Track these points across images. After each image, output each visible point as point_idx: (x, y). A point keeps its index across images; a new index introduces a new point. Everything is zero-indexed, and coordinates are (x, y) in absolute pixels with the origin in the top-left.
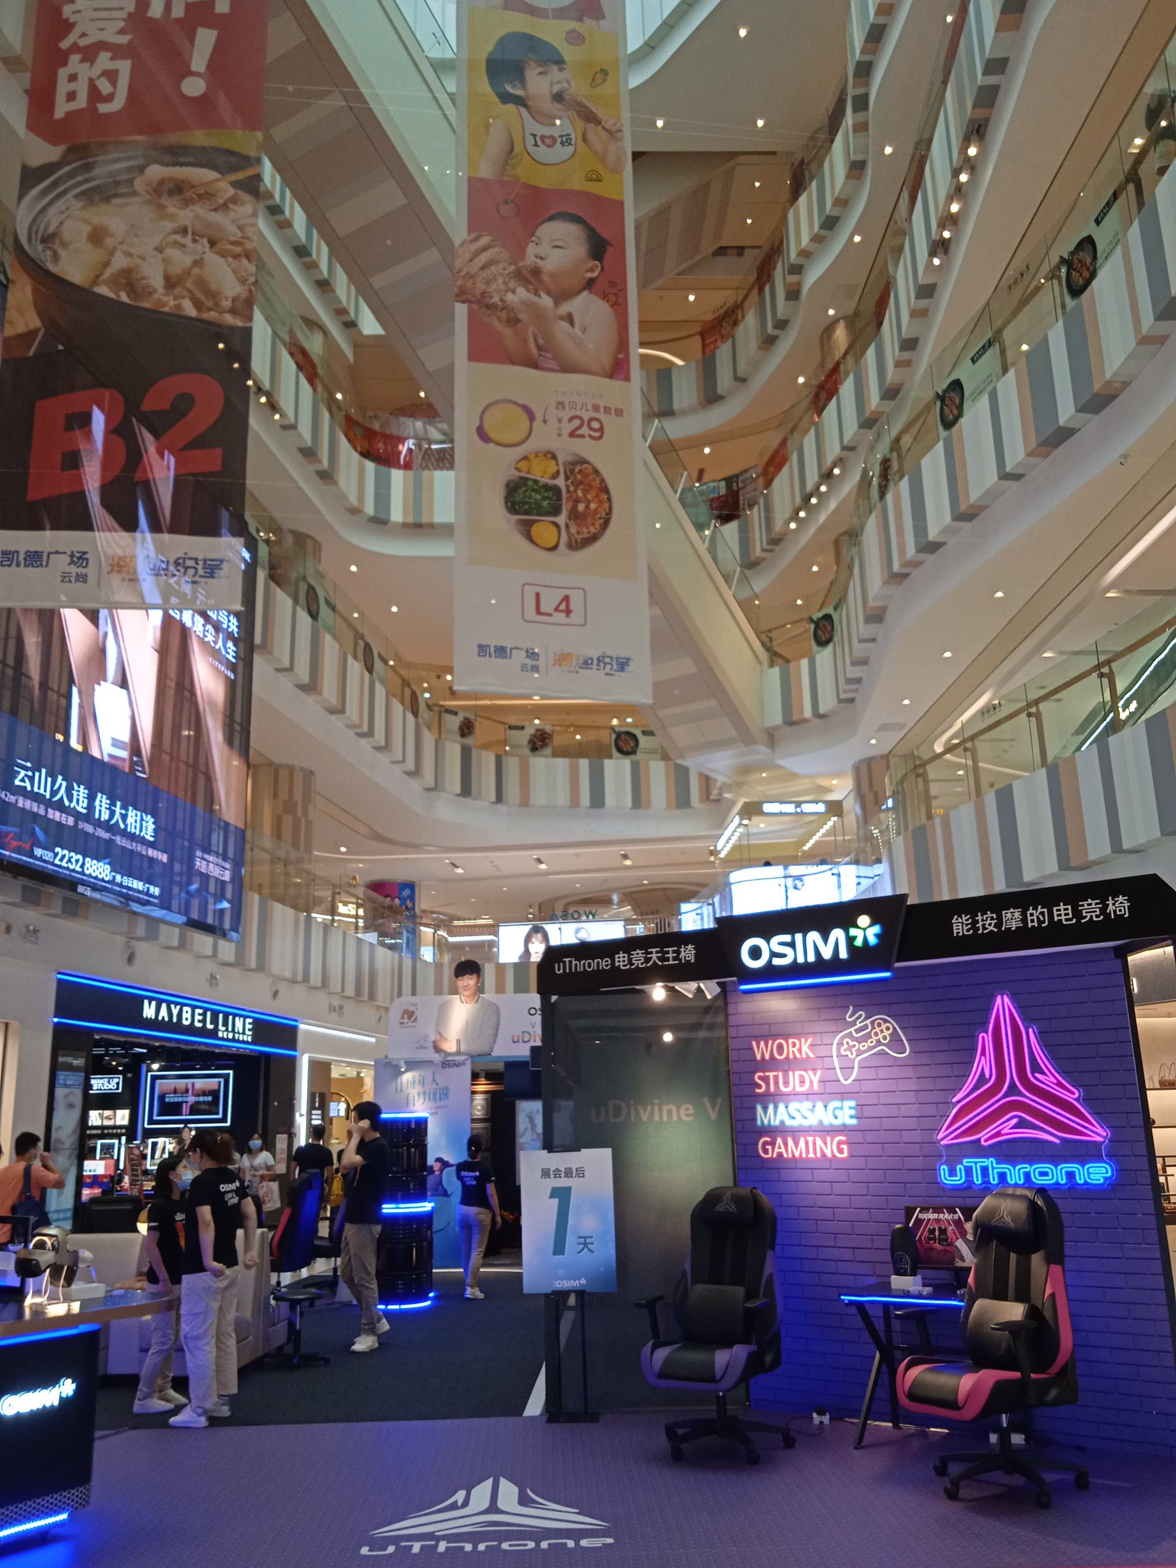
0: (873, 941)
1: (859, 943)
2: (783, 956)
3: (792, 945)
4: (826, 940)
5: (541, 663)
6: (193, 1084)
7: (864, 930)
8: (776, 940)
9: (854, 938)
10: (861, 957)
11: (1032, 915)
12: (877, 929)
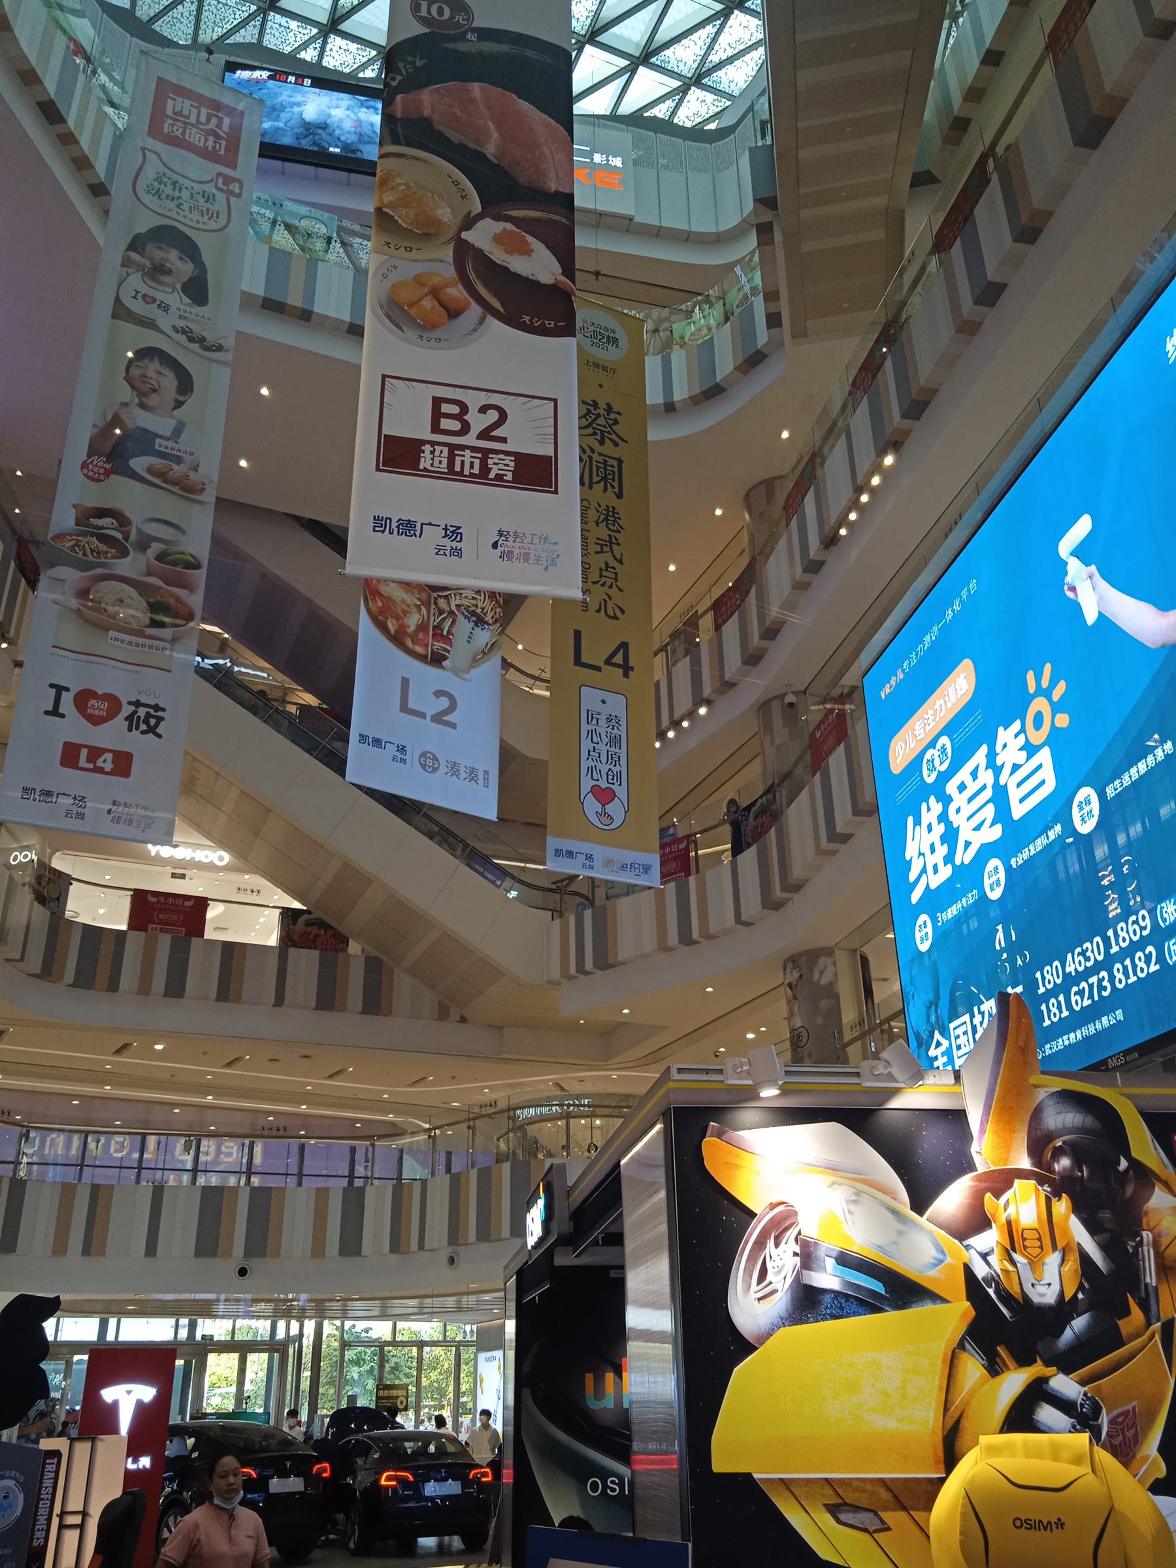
5: (408, 757)
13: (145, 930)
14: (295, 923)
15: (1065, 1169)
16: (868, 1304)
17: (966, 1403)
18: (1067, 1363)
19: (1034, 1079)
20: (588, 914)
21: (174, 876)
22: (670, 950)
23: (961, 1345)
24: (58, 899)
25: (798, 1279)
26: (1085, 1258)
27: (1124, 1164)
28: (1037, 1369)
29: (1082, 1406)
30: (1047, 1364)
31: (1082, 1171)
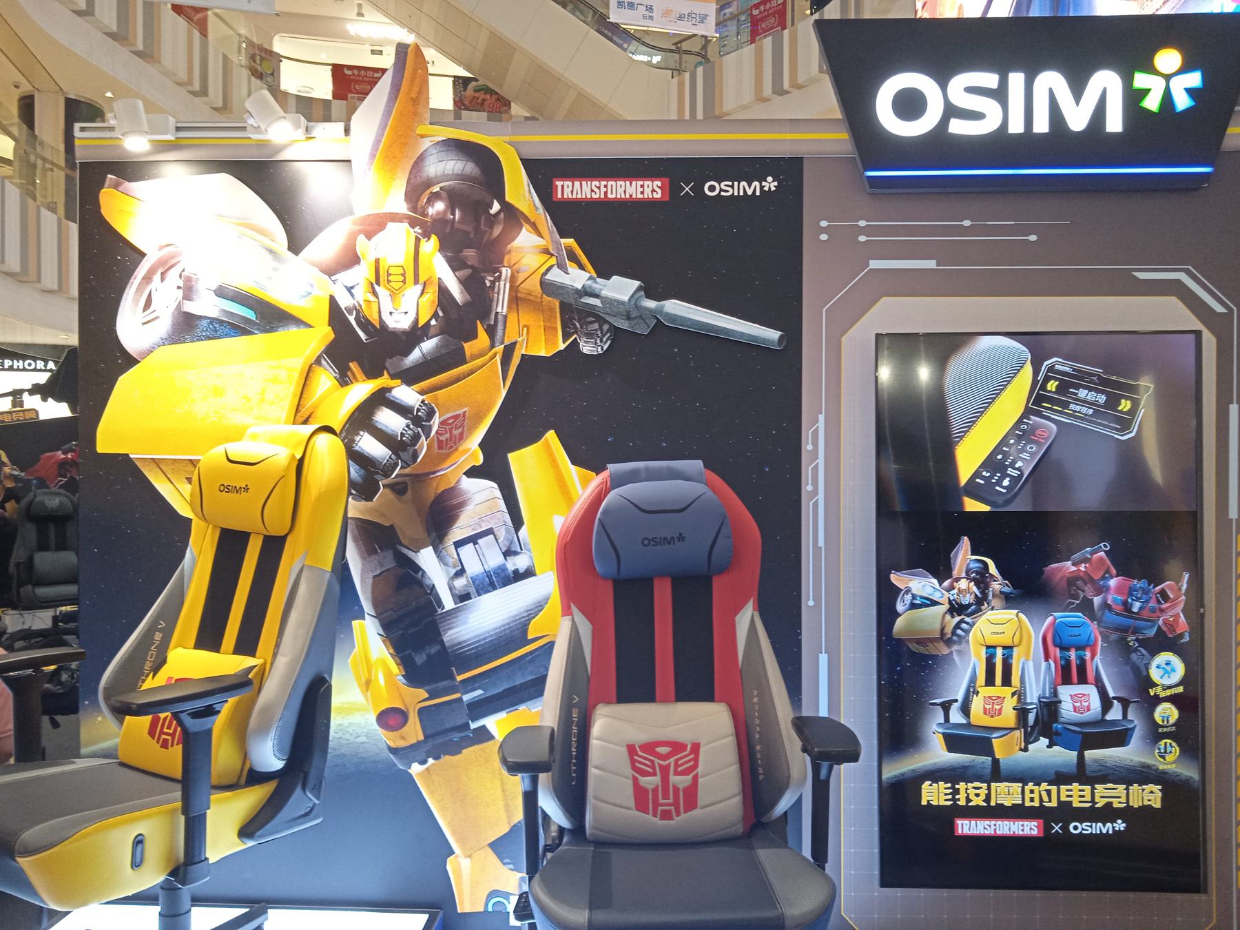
1: (1152, 103)
2: (977, 116)
3: (1000, 95)
4: (1078, 91)
6: (436, 398)
7: (1168, 78)
8: (960, 82)
9: (1144, 93)
10: (1151, 131)
13: (345, 98)
14: (465, 89)
15: (438, 213)
16: (239, 328)
17: (316, 407)
18: (410, 377)
19: (420, 130)
20: (700, 70)
21: (373, 52)
22: (766, 100)
23: (318, 361)
24: (272, 74)
25: (179, 306)
26: (443, 292)
27: (496, 207)
28: (384, 381)
29: (418, 410)
30: (393, 377)
31: (453, 214)
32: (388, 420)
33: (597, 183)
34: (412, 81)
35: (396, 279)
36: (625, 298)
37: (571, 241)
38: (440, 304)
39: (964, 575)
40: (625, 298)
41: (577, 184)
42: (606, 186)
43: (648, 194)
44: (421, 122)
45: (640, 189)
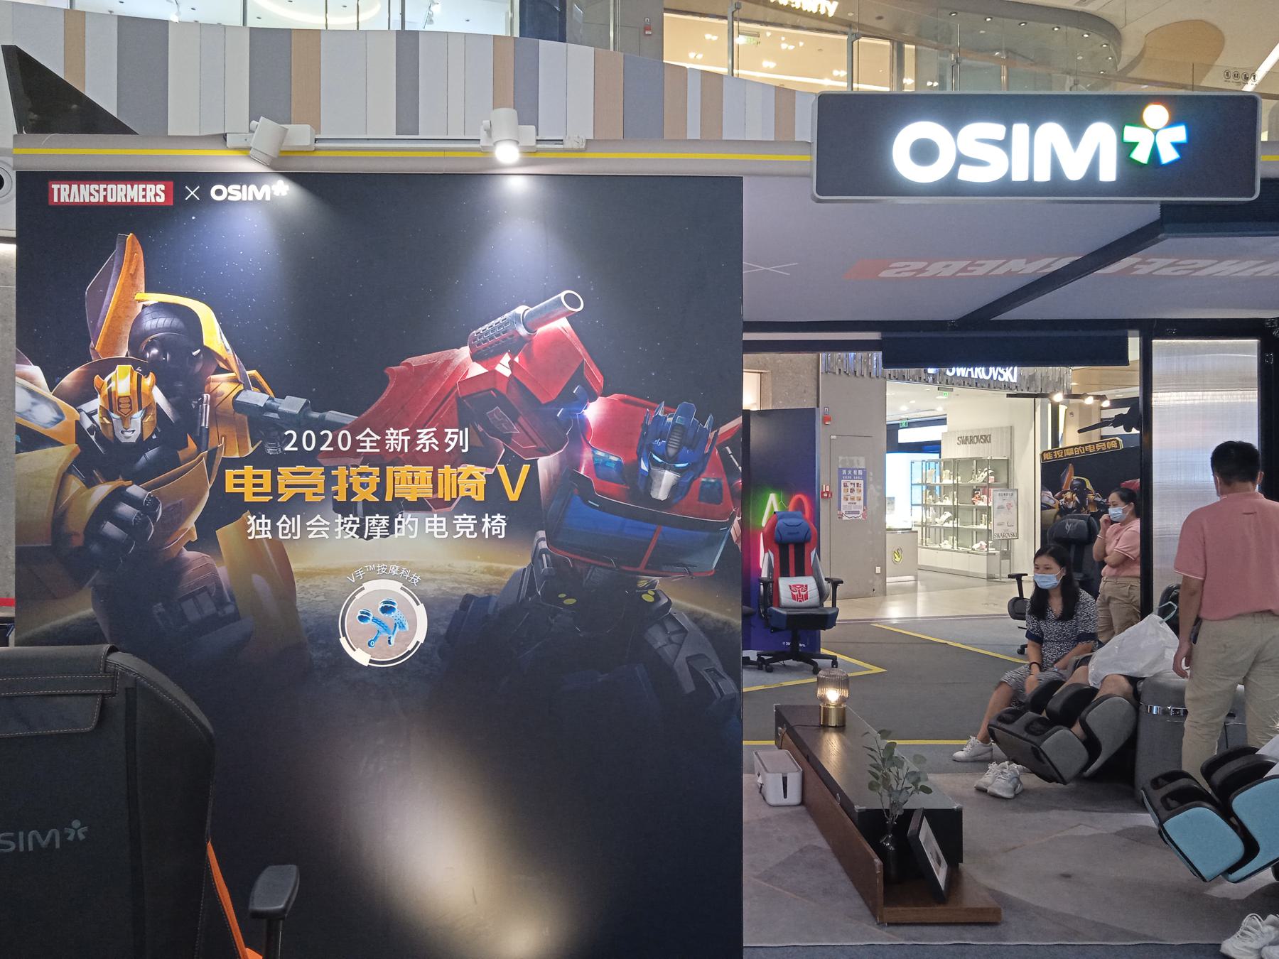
0: (1169, 155)
3: (1005, 144)
9: (1133, 146)
11: (400, 523)
12: (1180, 133)
17: (69, 503)
19: (138, 296)
26: (160, 411)
28: (119, 482)
32: (125, 509)
33: (96, 187)
34: (131, 261)
35: (124, 406)
36: (297, 412)
37: (253, 372)
38: (158, 424)
39: (124, 352)
40: (297, 412)
41: (75, 187)
42: (105, 190)
43: (150, 198)
44: (138, 291)
45: (142, 193)
